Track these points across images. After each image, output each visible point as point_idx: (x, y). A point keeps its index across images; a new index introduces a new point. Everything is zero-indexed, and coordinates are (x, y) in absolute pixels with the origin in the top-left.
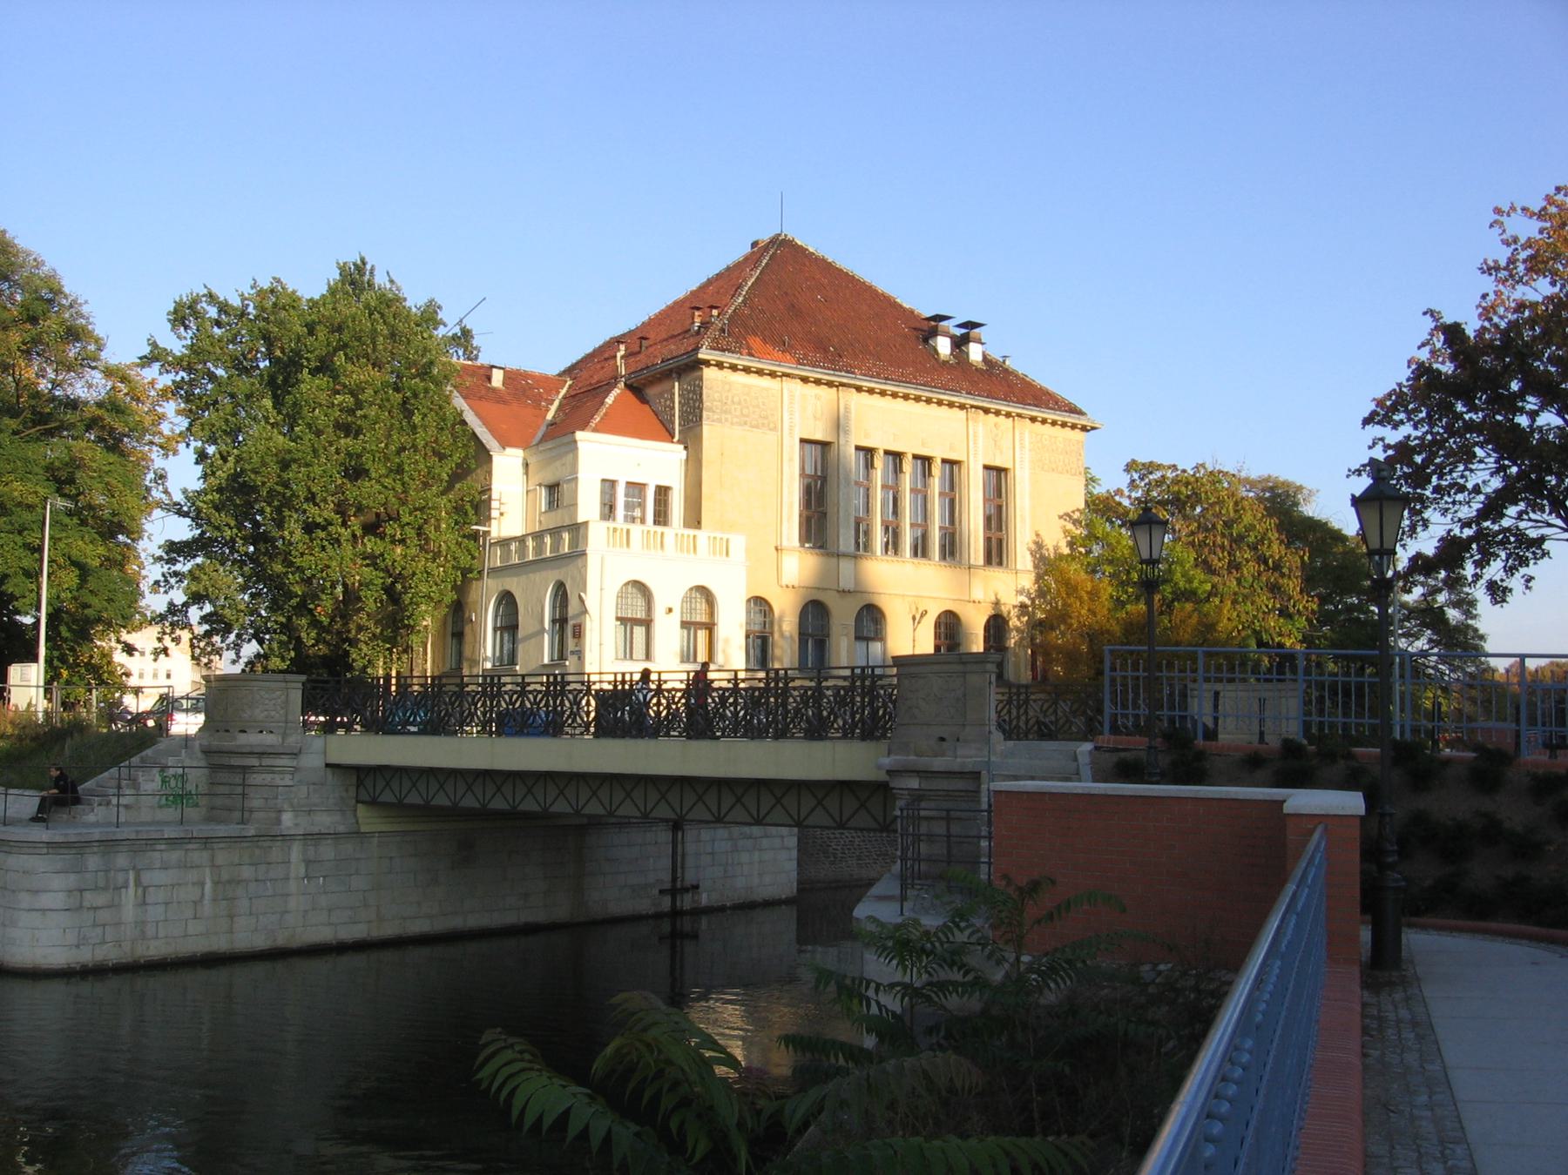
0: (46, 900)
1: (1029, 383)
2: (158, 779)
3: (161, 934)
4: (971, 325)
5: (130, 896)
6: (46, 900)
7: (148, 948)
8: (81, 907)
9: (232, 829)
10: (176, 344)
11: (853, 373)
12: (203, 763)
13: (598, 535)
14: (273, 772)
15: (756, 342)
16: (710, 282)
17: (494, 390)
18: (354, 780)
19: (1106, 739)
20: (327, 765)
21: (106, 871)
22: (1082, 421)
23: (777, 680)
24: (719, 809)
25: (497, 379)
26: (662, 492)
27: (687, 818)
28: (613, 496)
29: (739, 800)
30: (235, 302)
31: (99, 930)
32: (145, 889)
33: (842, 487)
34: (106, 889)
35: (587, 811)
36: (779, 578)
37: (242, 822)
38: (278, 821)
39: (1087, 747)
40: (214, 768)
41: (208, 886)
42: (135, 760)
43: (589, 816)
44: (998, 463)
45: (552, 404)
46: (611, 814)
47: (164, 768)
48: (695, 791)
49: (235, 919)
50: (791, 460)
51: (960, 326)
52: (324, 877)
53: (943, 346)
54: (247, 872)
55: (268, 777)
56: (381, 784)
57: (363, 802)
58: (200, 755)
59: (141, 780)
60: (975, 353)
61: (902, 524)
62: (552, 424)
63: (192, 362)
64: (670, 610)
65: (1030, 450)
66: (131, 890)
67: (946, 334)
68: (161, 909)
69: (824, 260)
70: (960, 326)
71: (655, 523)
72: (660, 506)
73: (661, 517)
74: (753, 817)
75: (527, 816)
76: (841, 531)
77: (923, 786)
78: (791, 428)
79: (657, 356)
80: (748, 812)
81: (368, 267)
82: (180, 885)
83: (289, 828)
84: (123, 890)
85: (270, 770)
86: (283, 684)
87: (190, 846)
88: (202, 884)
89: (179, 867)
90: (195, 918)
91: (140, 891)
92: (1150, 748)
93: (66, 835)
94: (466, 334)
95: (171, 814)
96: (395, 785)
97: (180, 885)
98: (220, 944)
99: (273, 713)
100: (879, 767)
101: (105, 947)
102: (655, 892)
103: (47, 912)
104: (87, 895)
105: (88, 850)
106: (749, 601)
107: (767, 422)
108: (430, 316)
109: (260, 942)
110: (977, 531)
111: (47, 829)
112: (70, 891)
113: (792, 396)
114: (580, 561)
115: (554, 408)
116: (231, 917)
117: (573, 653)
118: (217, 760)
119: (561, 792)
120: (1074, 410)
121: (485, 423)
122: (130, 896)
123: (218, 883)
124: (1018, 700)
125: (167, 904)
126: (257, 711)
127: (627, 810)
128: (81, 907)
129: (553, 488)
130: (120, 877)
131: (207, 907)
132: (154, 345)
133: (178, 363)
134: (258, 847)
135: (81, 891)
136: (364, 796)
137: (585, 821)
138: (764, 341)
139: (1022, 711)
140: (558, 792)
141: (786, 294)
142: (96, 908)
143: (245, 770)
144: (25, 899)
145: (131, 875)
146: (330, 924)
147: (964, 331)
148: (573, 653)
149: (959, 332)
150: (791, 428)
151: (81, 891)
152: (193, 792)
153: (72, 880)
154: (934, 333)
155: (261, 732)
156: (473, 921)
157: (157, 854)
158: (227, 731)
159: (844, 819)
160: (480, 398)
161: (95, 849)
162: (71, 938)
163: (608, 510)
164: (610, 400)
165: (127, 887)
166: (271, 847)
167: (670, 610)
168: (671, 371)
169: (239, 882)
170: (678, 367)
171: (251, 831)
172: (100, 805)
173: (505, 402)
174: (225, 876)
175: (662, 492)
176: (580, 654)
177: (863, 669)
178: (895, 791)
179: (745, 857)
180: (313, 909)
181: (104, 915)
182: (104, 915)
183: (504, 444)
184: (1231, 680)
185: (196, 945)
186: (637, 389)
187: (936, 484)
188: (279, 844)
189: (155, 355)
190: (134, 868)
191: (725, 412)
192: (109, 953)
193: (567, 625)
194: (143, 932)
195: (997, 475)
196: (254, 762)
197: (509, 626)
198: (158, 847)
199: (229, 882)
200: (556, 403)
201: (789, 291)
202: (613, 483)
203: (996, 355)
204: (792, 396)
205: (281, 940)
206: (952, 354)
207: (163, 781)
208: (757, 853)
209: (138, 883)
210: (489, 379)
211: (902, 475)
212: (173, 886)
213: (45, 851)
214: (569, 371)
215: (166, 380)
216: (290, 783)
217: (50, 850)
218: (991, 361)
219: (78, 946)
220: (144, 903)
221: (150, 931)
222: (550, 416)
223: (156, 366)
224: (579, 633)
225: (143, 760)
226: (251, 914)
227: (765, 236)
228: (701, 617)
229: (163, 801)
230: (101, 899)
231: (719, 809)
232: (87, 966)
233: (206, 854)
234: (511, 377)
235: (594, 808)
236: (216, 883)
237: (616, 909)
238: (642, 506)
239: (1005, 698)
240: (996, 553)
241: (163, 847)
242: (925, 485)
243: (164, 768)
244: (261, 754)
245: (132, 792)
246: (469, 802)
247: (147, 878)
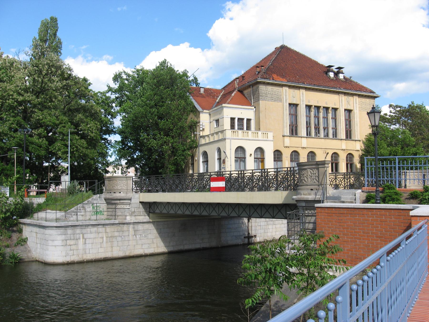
0: (56, 243)
1: (358, 84)
2: (91, 207)
3: (91, 252)
4: (340, 68)
5: (81, 241)
6: (56, 243)
7: (87, 256)
8: (66, 245)
9: (112, 221)
10: (115, 86)
11: (304, 83)
12: (105, 202)
13: (229, 133)
14: (124, 205)
15: (275, 76)
16: (263, 60)
17: (201, 94)
18: (148, 206)
19: (366, 188)
20: (140, 202)
21: (74, 234)
22: (375, 95)
23: (265, 172)
24: (250, 213)
25: (202, 91)
26: (249, 120)
27: (241, 216)
28: (234, 123)
29: (280, 211)
30: (131, 73)
31: (72, 251)
32: (85, 239)
33: (302, 117)
34: (74, 239)
35: (221, 215)
36: (284, 144)
37: (115, 219)
38: (125, 219)
39: (360, 191)
40: (108, 203)
41: (105, 238)
42: (86, 202)
43: (222, 216)
44: (349, 108)
45: (218, 97)
46: (219, 215)
47: (93, 204)
48: (277, 208)
49: (113, 248)
50: (286, 110)
51: (336, 69)
52: (140, 235)
53: (332, 75)
54: (116, 234)
55: (122, 206)
56: (241, 210)
57: (151, 213)
58: (104, 200)
59: (86, 207)
60: (341, 76)
61: (320, 127)
62: (218, 103)
63: (120, 89)
64: (251, 155)
65: (359, 104)
66: (81, 240)
67: (332, 71)
68: (91, 245)
69: (296, 52)
70: (336, 69)
71: (247, 129)
72: (248, 124)
73: (248, 128)
74: (260, 216)
75: (195, 216)
76: (302, 130)
77: (307, 205)
78: (286, 100)
79: (246, 82)
80: (283, 215)
81: (167, 62)
82: (96, 238)
83: (128, 221)
84: (79, 240)
85: (123, 204)
86: (126, 179)
87: (99, 227)
88: (103, 238)
89: (96, 233)
90: (101, 247)
91: (84, 240)
92: (376, 191)
93: (61, 224)
94: (196, 79)
95: (94, 217)
96: (227, 210)
97: (96, 238)
98: (109, 255)
99: (123, 187)
100: (293, 199)
101: (74, 256)
102: (243, 237)
103: (57, 247)
104: (68, 241)
105: (67, 228)
106: (274, 152)
107: (279, 99)
108: (185, 74)
109: (121, 254)
110: (343, 127)
111: (56, 222)
112: (63, 240)
113: (303, 94)
114: (224, 142)
115: (219, 98)
116: (112, 247)
117: (223, 168)
118: (108, 201)
119: (244, 210)
120: (372, 92)
121: (198, 103)
122: (81, 241)
123: (107, 237)
124: (347, 177)
125: (92, 243)
126: (119, 187)
127: (234, 214)
128: (66, 245)
129: (217, 121)
130: (78, 236)
131: (105, 245)
132: (109, 87)
133: (116, 91)
134: (119, 226)
135: (66, 240)
136: (151, 211)
137: (220, 217)
138: (277, 75)
139: (348, 181)
140: (266, 210)
141: (284, 62)
142: (70, 245)
143: (115, 204)
144: (50, 243)
145: (81, 235)
146: (142, 249)
147: (338, 70)
148: (223, 168)
149: (336, 70)
150: (286, 100)
151: (66, 240)
152: (102, 211)
153: (63, 237)
154: (329, 71)
155: (120, 193)
156: (186, 247)
157: (89, 229)
158: (110, 193)
159: (274, 216)
160: (197, 96)
161: (70, 228)
162: (64, 254)
163: (232, 127)
164: (233, 95)
165: (80, 239)
166: (123, 226)
167: (251, 155)
168: (250, 85)
169: (114, 237)
170: (252, 84)
171: (117, 222)
172: (74, 215)
173: (204, 97)
174: (110, 235)
175: (249, 120)
176: (224, 168)
177: (290, 168)
178: (298, 207)
179: (270, 227)
180: (137, 244)
181: (73, 247)
182: (73, 247)
183: (204, 108)
184: (412, 169)
185: (102, 255)
186: (241, 91)
187: (330, 115)
188: (126, 225)
189: (110, 89)
190: (82, 233)
191: (266, 97)
192: (75, 258)
193: (221, 161)
194: (85, 252)
195: (349, 111)
196: (118, 202)
197: (206, 161)
198: (89, 227)
199: (111, 237)
200: (220, 97)
201: (285, 61)
202: (243, 119)
203: (348, 76)
204: (303, 94)
205: (128, 254)
206: (334, 77)
207: (93, 208)
208: (274, 225)
209: (83, 238)
210: (200, 91)
211: (329, 114)
212: (94, 238)
213: (55, 229)
214: (224, 88)
215: (113, 97)
216: (129, 208)
217: (57, 229)
218: (346, 78)
219: (66, 256)
220: (85, 243)
221: (87, 251)
222: (217, 101)
223: (110, 92)
224: (224, 162)
225: (88, 202)
226: (118, 246)
227: (278, 45)
228: (259, 156)
229: (93, 214)
230: (72, 242)
231: (250, 213)
232: (69, 262)
233: (104, 229)
234: (206, 90)
235: (224, 214)
236: (107, 237)
237: (231, 242)
238: (243, 125)
239: (343, 177)
240: (349, 135)
241: (90, 227)
242: (327, 115)
243: (93, 204)
244: (120, 200)
245: (84, 211)
246: (180, 212)
247: (86, 236)
